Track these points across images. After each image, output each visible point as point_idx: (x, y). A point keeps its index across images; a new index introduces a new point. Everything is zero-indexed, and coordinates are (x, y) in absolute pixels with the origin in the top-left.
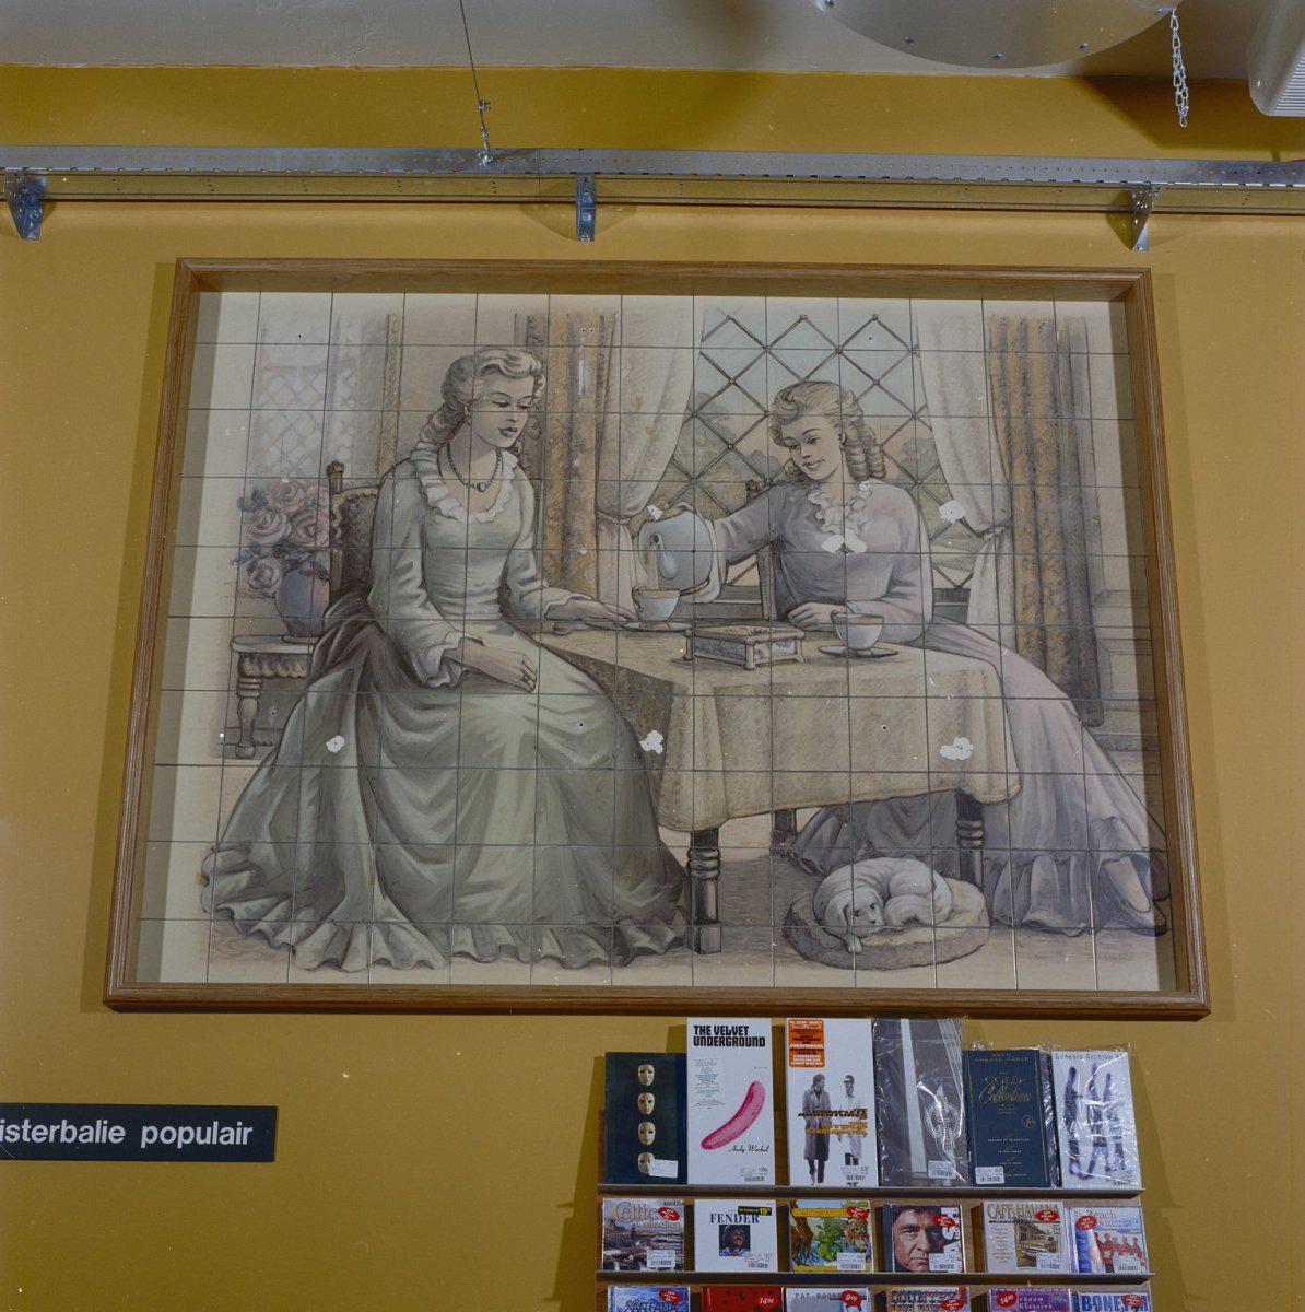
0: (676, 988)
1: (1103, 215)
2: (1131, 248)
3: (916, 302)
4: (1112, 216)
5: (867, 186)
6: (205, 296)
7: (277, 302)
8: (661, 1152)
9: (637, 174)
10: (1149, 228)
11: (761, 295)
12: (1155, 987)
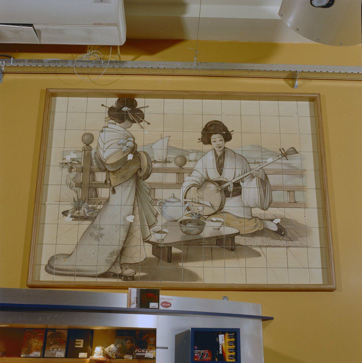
0: (259, 284)
1: (283, 79)
2: (293, 88)
3: (242, 101)
4: (286, 80)
5: (310, 74)
6: (53, 98)
7: (74, 101)
8: (119, 337)
9: (207, 69)
10: (297, 83)
11: (67, 97)
12: (321, 283)
